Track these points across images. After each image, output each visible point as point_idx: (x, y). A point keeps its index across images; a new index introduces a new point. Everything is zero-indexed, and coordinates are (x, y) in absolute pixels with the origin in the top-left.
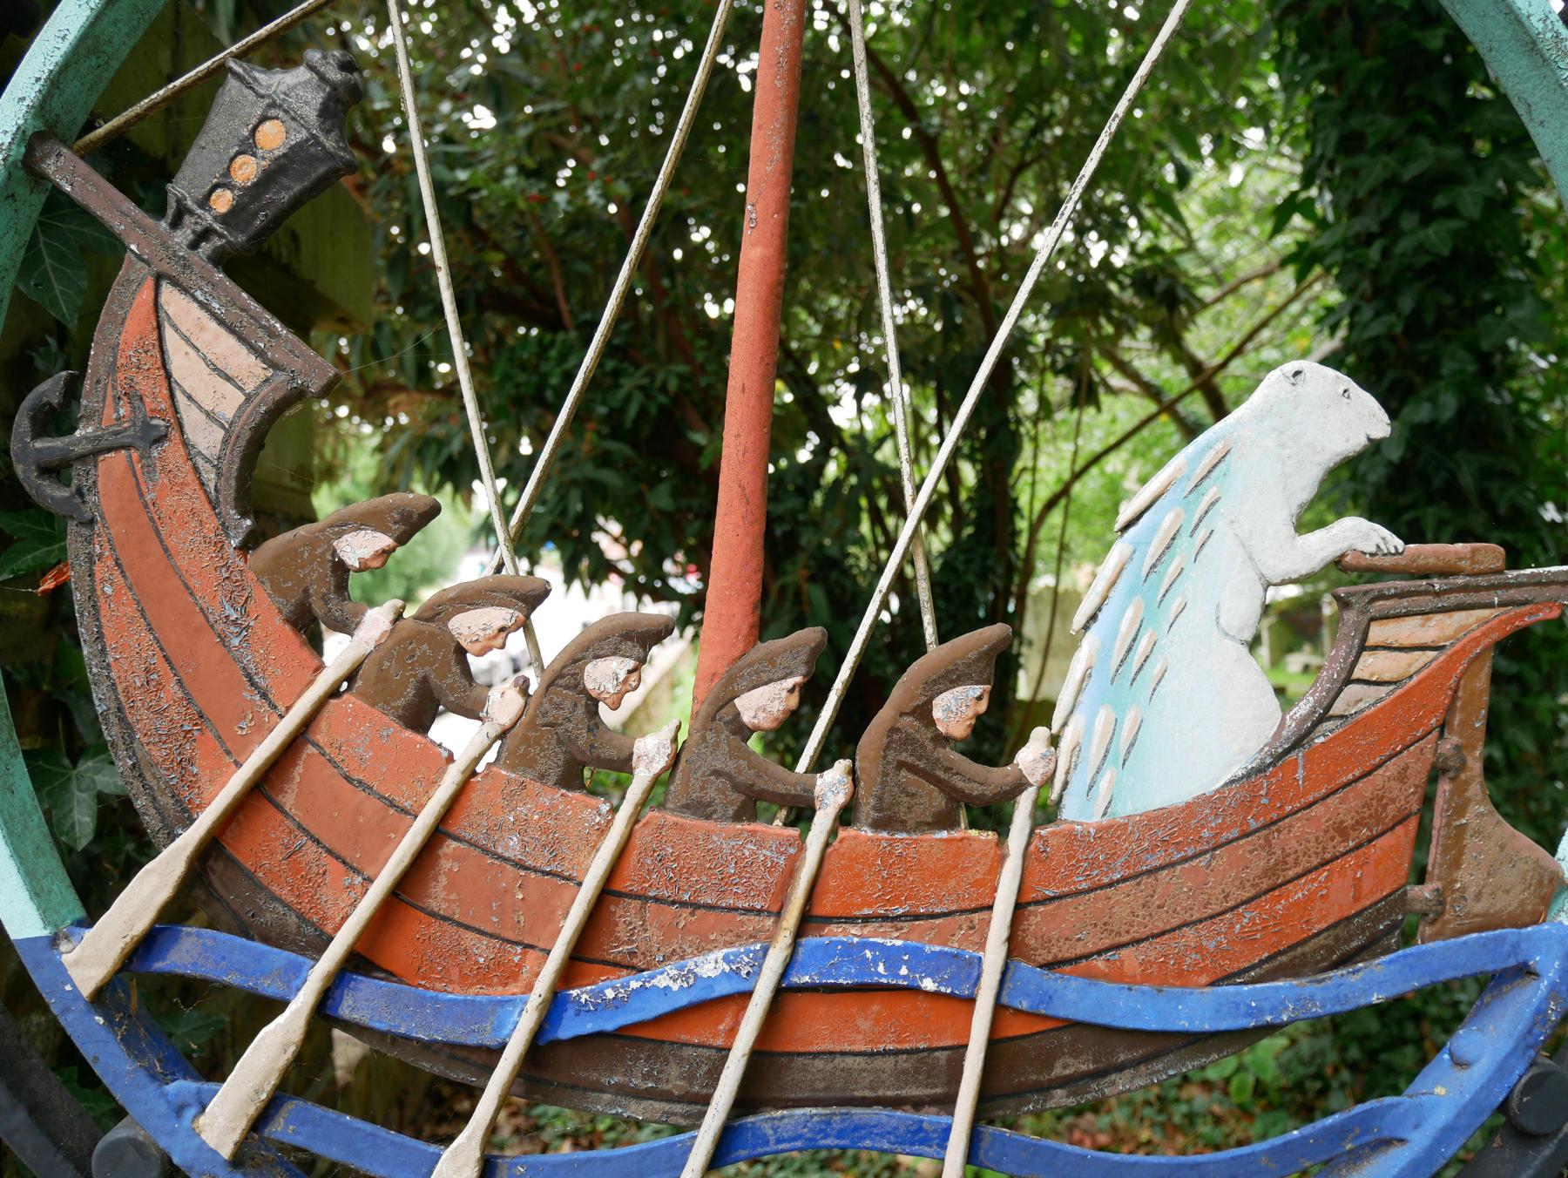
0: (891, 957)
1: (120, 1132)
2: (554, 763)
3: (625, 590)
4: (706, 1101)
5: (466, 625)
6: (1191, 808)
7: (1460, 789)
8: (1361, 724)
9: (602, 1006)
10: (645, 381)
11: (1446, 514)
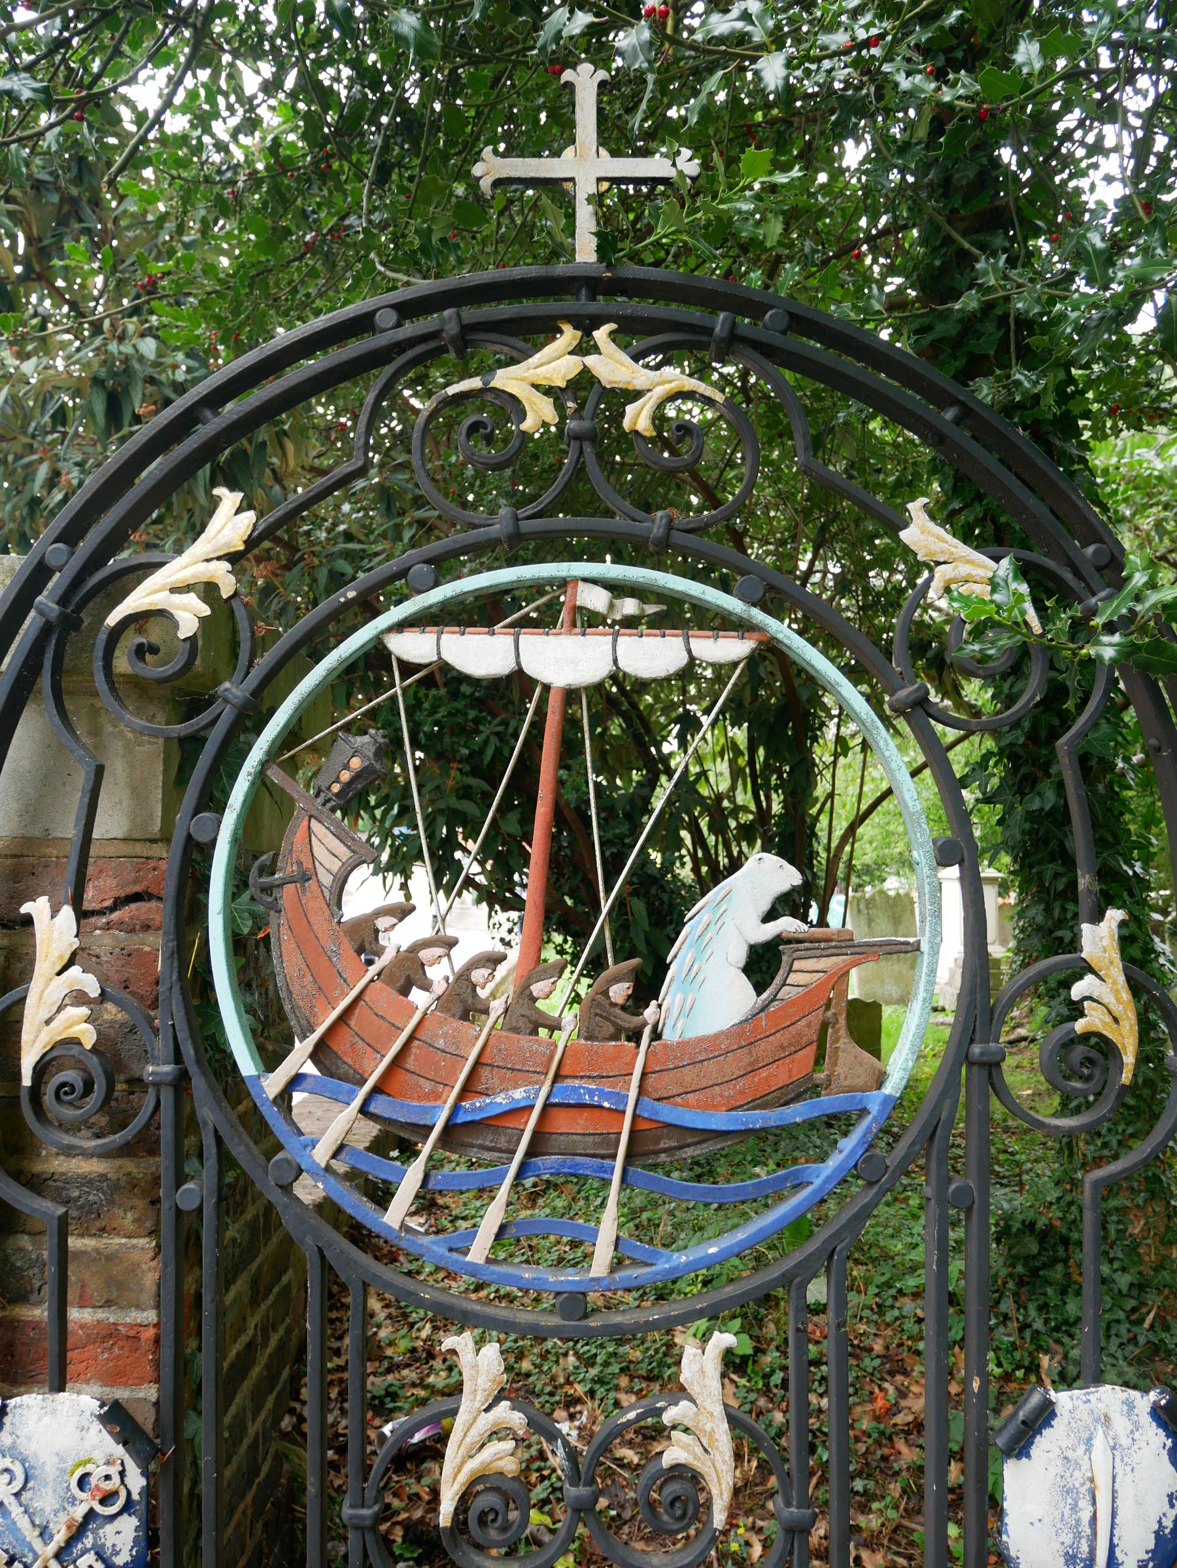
0: (591, 1093)
1: (280, 1156)
2: (458, 1009)
3: (478, 901)
4: (514, 1152)
5: (425, 955)
6: (717, 1036)
7: (836, 1032)
8: (792, 1003)
9: (475, 1110)
10: (500, 729)
11: (1061, 869)
